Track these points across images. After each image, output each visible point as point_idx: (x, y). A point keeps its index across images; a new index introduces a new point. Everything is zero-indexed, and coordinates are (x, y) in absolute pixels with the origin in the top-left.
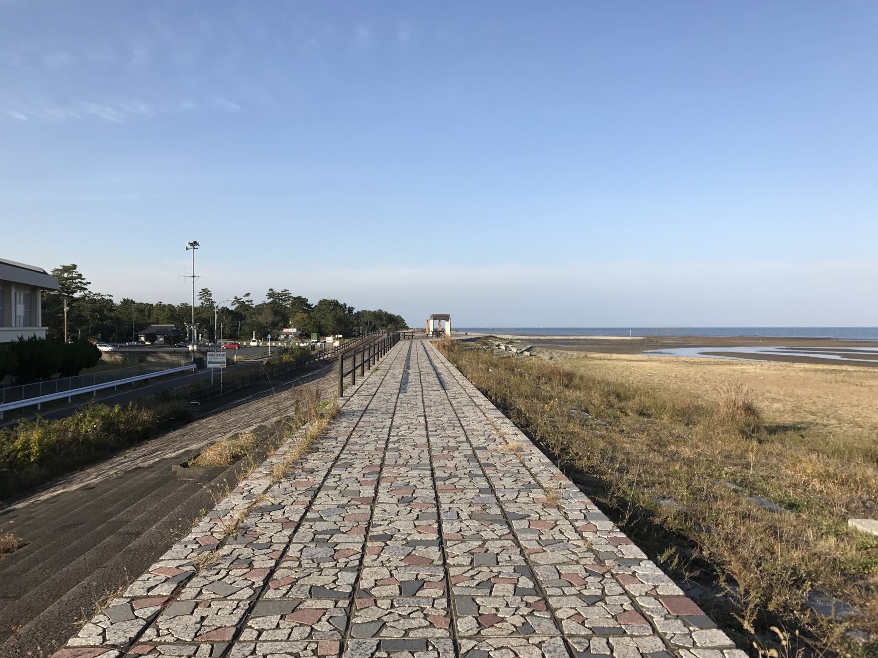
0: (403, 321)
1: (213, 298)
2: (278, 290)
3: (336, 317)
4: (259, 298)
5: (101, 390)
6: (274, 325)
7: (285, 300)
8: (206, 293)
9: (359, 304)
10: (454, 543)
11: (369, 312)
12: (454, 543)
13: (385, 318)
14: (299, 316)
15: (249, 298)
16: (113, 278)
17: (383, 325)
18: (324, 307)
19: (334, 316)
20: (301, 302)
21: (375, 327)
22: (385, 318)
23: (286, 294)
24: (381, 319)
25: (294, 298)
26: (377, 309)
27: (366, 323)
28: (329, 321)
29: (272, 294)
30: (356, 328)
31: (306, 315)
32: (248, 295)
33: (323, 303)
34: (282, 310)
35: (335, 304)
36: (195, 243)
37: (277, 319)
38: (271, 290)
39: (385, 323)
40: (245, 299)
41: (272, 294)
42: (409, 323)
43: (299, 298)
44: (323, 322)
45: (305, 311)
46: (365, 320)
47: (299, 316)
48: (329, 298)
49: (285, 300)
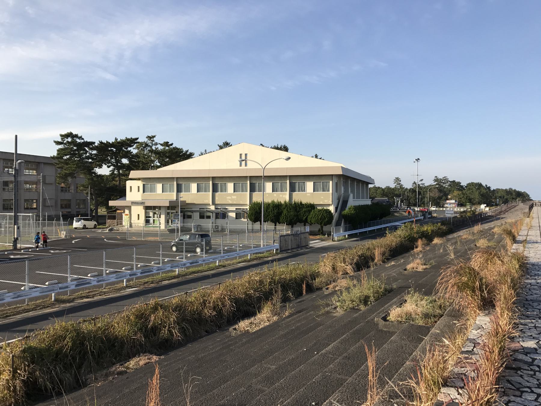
0: (529, 196)
1: (402, 183)
2: (440, 177)
3: (483, 194)
4: (429, 181)
5: (143, 169)
6: (440, 198)
7: (444, 183)
8: (397, 180)
9: (495, 183)
10: (514, 388)
11: (502, 190)
12: (514, 388)
13: (514, 194)
14: (456, 193)
15: (423, 182)
16: (382, 176)
17: (513, 199)
18: (472, 187)
19: (479, 193)
20: (455, 185)
21: (507, 199)
22: (514, 194)
23: (446, 180)
24: (511, 194)
25: (451, 182)
26: (508, 188)
27: (500, 197)
28: (476, 196)
29: (436, 180)
30: (493, 200)
31: (461, 192)
32: (422, 180)
33: (469, 185)
34: (443, 190)
35: (480, 185)
36: (418, 159)
37: (442, 195)
38: (436, 177)
39: (514, 197)
40: (420, 183)
41: (436, 180)
42: (532, 197)
43: (454, 181)
44: (472, 197)
45: (459, 190)
46: (499, 195)
47: (456, 193)
48: (475, 181)
49: (444, 183)
